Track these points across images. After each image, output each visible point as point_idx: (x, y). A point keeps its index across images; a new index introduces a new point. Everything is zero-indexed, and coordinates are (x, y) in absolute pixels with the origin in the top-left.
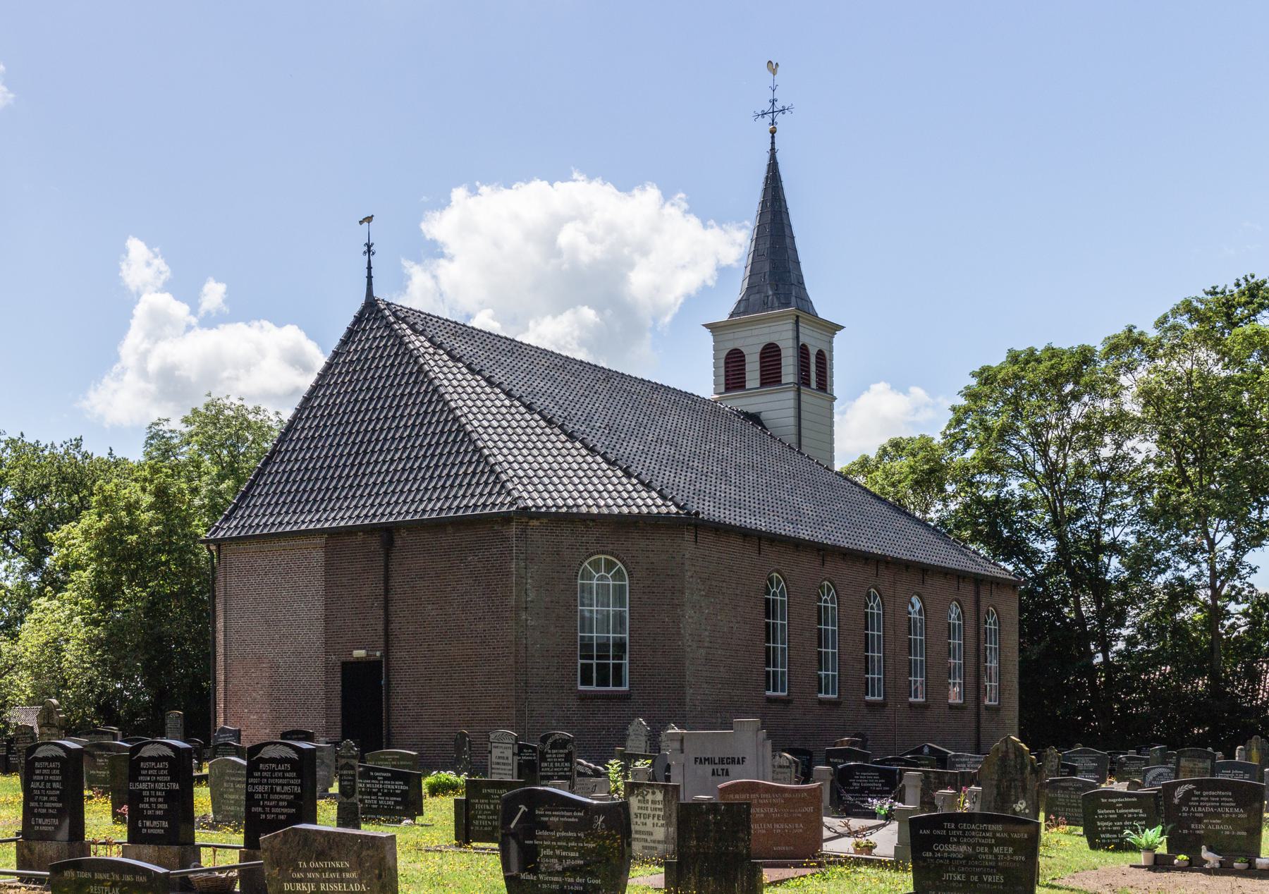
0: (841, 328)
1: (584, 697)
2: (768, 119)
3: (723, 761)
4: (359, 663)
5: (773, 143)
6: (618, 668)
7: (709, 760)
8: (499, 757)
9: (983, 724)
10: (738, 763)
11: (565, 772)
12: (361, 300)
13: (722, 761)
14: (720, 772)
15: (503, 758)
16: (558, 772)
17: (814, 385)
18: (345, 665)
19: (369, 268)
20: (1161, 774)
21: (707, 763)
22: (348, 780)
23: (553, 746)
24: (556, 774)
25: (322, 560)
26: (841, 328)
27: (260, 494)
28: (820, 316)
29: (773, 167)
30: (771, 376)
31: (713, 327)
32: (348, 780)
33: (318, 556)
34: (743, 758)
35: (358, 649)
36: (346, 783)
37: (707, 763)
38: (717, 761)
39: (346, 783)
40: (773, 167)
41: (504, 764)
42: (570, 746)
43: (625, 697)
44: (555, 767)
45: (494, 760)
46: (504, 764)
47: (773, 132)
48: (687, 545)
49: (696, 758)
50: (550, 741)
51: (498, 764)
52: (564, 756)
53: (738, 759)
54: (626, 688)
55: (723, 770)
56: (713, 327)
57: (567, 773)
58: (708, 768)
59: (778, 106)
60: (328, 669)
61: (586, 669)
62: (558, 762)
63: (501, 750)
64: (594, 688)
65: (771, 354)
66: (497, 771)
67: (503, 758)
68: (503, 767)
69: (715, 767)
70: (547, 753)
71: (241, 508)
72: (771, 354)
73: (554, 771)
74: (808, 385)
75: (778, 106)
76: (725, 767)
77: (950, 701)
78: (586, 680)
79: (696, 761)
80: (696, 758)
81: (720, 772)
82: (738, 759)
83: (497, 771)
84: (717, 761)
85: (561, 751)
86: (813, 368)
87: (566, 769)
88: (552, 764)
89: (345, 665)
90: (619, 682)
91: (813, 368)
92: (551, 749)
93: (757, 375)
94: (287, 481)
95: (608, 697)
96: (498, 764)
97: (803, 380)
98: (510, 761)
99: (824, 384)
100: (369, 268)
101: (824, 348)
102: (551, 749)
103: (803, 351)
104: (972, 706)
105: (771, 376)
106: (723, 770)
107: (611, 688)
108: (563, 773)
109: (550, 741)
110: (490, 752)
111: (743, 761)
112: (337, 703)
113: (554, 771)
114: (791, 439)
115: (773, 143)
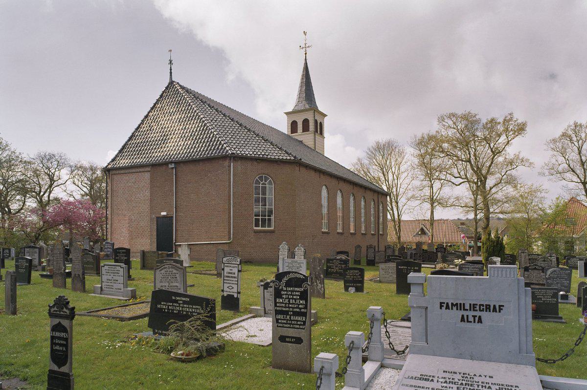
0: (326, 116)
1: (256, 232)
2: (304, 49)
3: (474, 307)
4: (164, 217)
5: (306, 57)
6: (269, 220)
7: (460, 306)
8: (229, 273)
9: (380, 240)
10: (495, 310)
11: (300, 309)
12: (168, 81)
13: (473, 307)
14: (471, 319)
15: (231, 273)
16: (293, 308)
17: (319, 132)
18: (157, 218)
19: (171, 69)
20: (555, 271)
21: (455, 308)
22: (61, 345)
23: (288, 284)
24: (291, 309)
25: (149, 177)
26: (326, 116)
27: (126, 152)
28: (320, 109)
29: (306, 64)
30: (306, 128)
31: (287, 114)
32: (61, 345)
33: (147, 176)
34: (500, 306)
35: (163, 212)
36: (57, 348)
37: (455, 308)
38: (467, 307)
39: (57, 348)
40: (306, 64)
41: (232, 277)
42: (304, 285)
43: (272, 232)
44: (289, 304)
45: (226, 274)
46: (232, 277)
47: (306, 54)
48: (297, 171)
49: (441, 303)
50: (285, 279)
51: (228, 277)
52: (299, 293)
53: (494, 306)
54: (272, 228)
55: (474, 317)
56: (287, 114)
57: (303, 310)
58: (457, 314)
59: (307, 45)
60: (151, 219)
61: (257, 221)
62: (293, 299)
63: (231, 268)
64: (260, 228)
65: (306, 122)
66: (228, 282)
67: (231, 273)
68: (231, 279)
69: (465, 313)
70: (282, 290)
71: (118, 157)
72: (306, 122)
73: (289, 307)
74: (317, 132)
75: (307, 45)
76: (478, 314)
77: (338, 231)
78: (257, 225)
79: (441, 307)
80: (441, 303)
81: (471, 319)
82: (494, 306)
83: (228, 282)
84: (467, 307)
85: (296, 289)
86: (319, 127)
87: (300, 306)
88: (287, 301)
89: (157, 218)
90: (269, 226)
91: (319, 127)
92: (286, 286)
93: (301, 128)
94: (137, 147)
95: (264, 232)
96: (228, 277)
97: (316, 131)
98: (236, 275)
99: (321, 133)
100: (171, 69)
101: (322, 121)
102: (286, 286)
103: (316, 121)
104: (377, 233)
105: (306, 128)
106: (474, 317)
107: (267, 228)
108: (298, 310)
109: (285, 279)
110: (223, 269)
111: (500, 310)
112: (155, 233)
113: (289, 307)
114: (313, 148)
115: (306, 57)
